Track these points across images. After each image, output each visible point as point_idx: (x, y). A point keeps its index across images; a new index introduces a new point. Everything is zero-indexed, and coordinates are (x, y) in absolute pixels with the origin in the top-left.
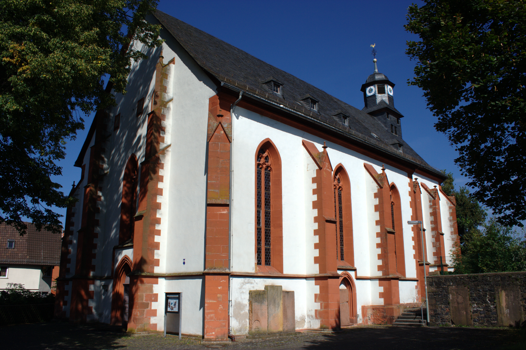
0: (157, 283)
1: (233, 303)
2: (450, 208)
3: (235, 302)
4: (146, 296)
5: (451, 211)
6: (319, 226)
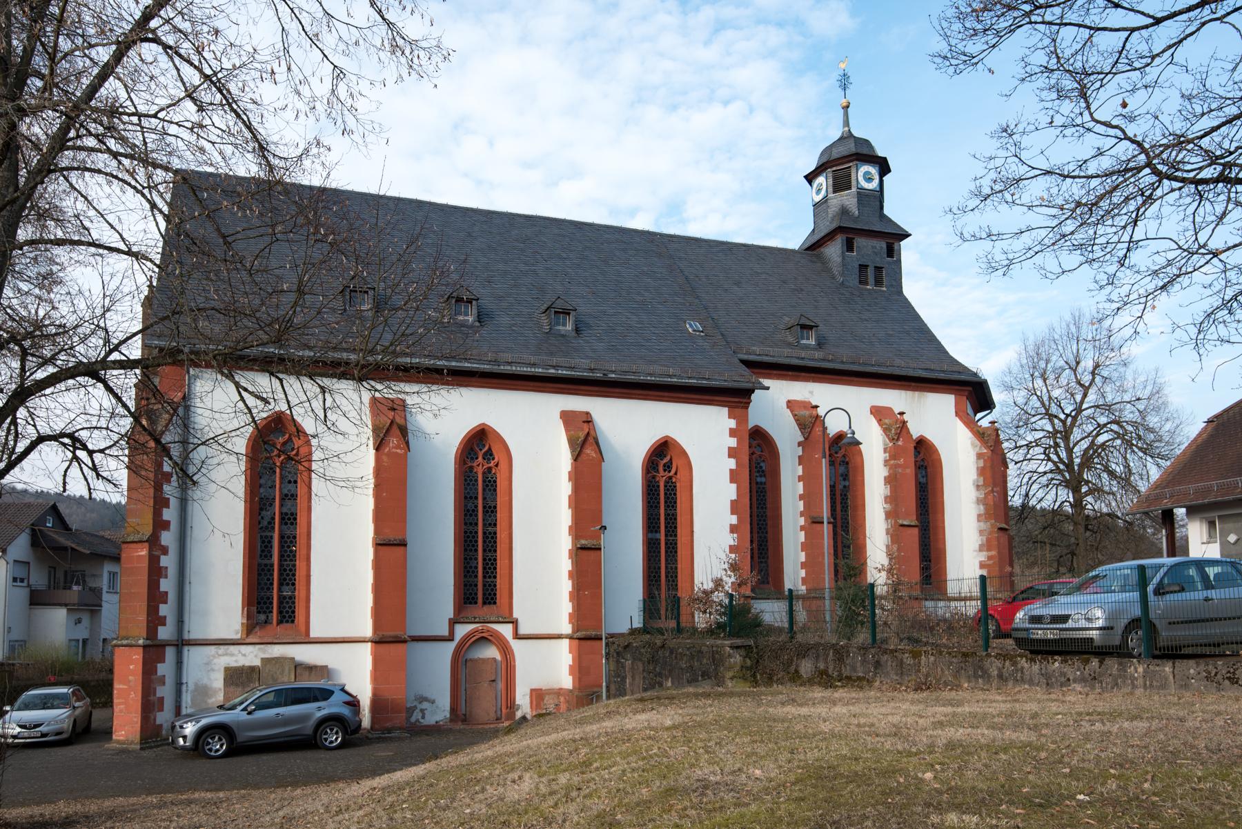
1: (191, 686)
2: (979, 456)
3: (196, 685)
5: (981, 464)
6: (739, 519)
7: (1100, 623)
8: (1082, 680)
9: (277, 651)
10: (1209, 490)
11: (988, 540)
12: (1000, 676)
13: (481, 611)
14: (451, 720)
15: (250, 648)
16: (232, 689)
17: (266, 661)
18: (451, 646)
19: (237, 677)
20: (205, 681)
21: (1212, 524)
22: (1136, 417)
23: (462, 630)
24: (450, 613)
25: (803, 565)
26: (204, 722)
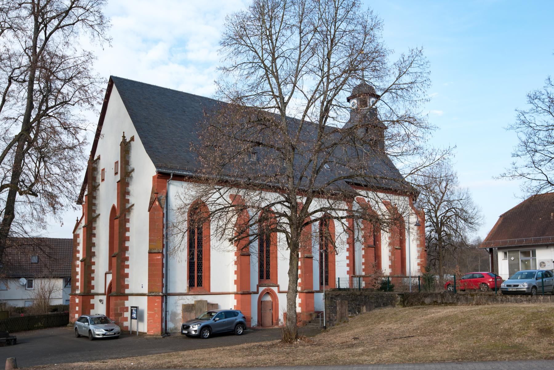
0: (128, 300)
1: (170, 312)
4: (121, 309)
7: (526, 287)
8: (526, 301)
9: (200, 298)
10: (506, 242)
11: (421, 255)
12: (502, 301)
13: (267, 282)
14: (258, 325)
15: (190, 296)
16: (186, 313)
17: (198, 302)
18: (258, 296)
19: (188, 308)
20: (175, 310)
21: (505, 253)
22: (460, 207)
23: (261, 289)
24: (257, 283)
25: (363, 264)
26: (203, 324)
